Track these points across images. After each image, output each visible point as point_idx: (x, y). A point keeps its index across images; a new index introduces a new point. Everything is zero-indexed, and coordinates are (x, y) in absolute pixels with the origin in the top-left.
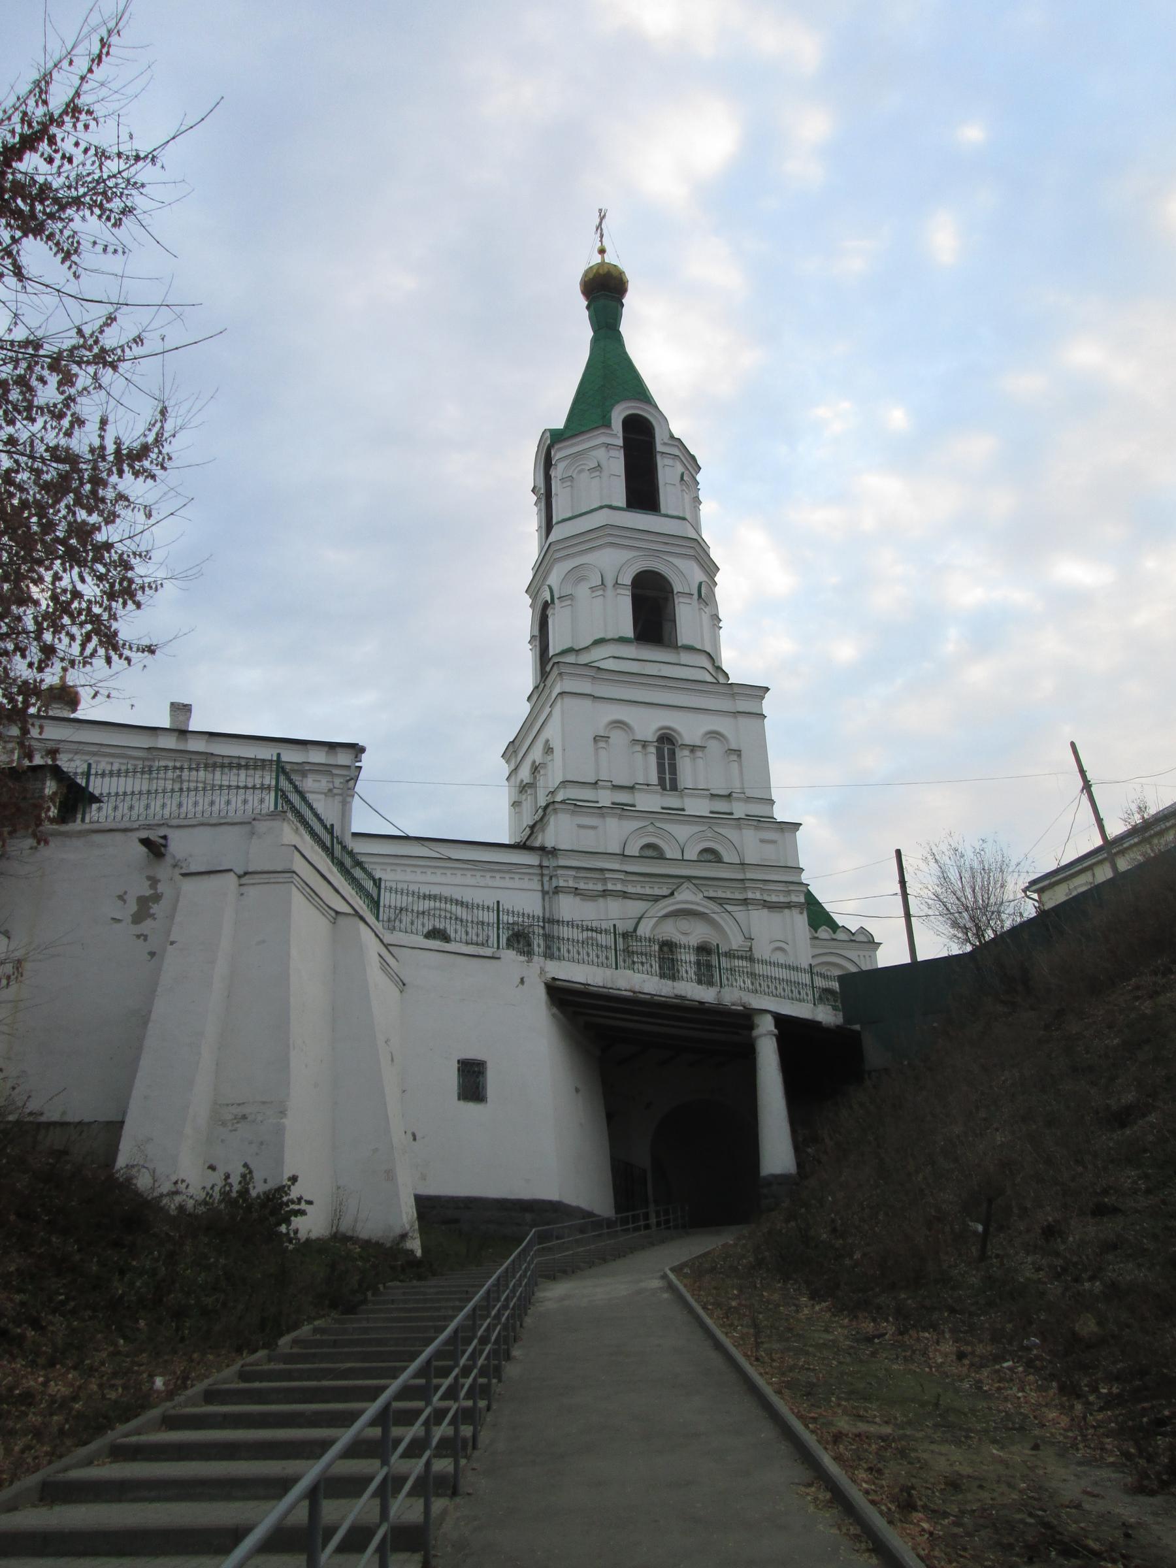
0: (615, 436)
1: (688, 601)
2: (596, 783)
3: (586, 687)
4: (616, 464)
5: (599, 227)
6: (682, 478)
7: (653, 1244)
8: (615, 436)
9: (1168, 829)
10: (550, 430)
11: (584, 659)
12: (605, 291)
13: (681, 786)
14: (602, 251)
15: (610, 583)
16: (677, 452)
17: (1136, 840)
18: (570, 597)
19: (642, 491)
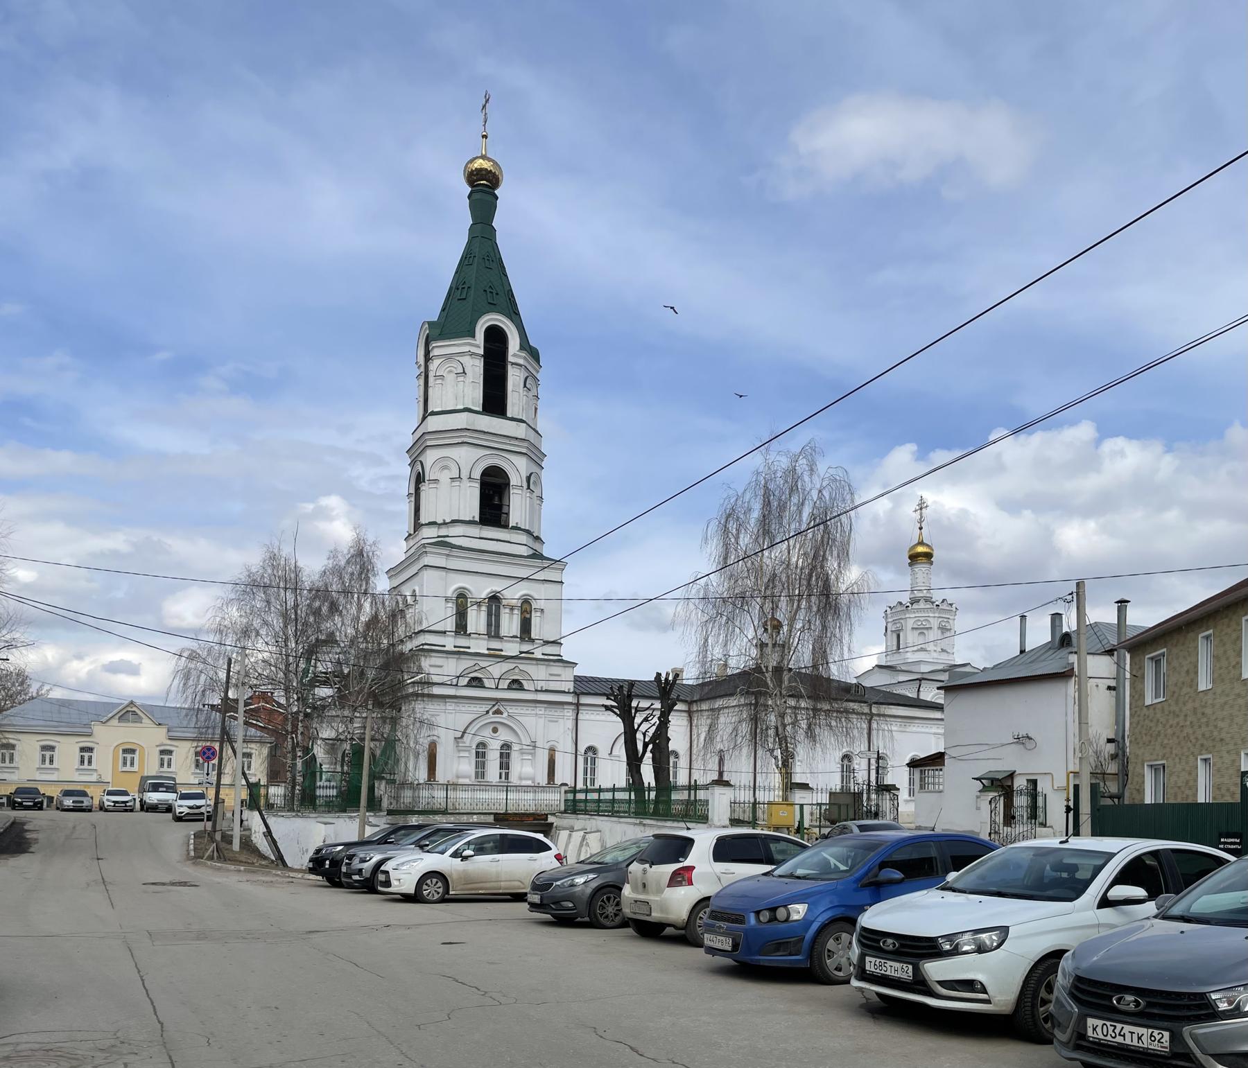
3: (441, 562)
4: (476, 368)
5: (487, 101)
9: (371, 789)
10: (429, 323)
12: (483, 185)
15: (465, 474)
18: (436, 481)
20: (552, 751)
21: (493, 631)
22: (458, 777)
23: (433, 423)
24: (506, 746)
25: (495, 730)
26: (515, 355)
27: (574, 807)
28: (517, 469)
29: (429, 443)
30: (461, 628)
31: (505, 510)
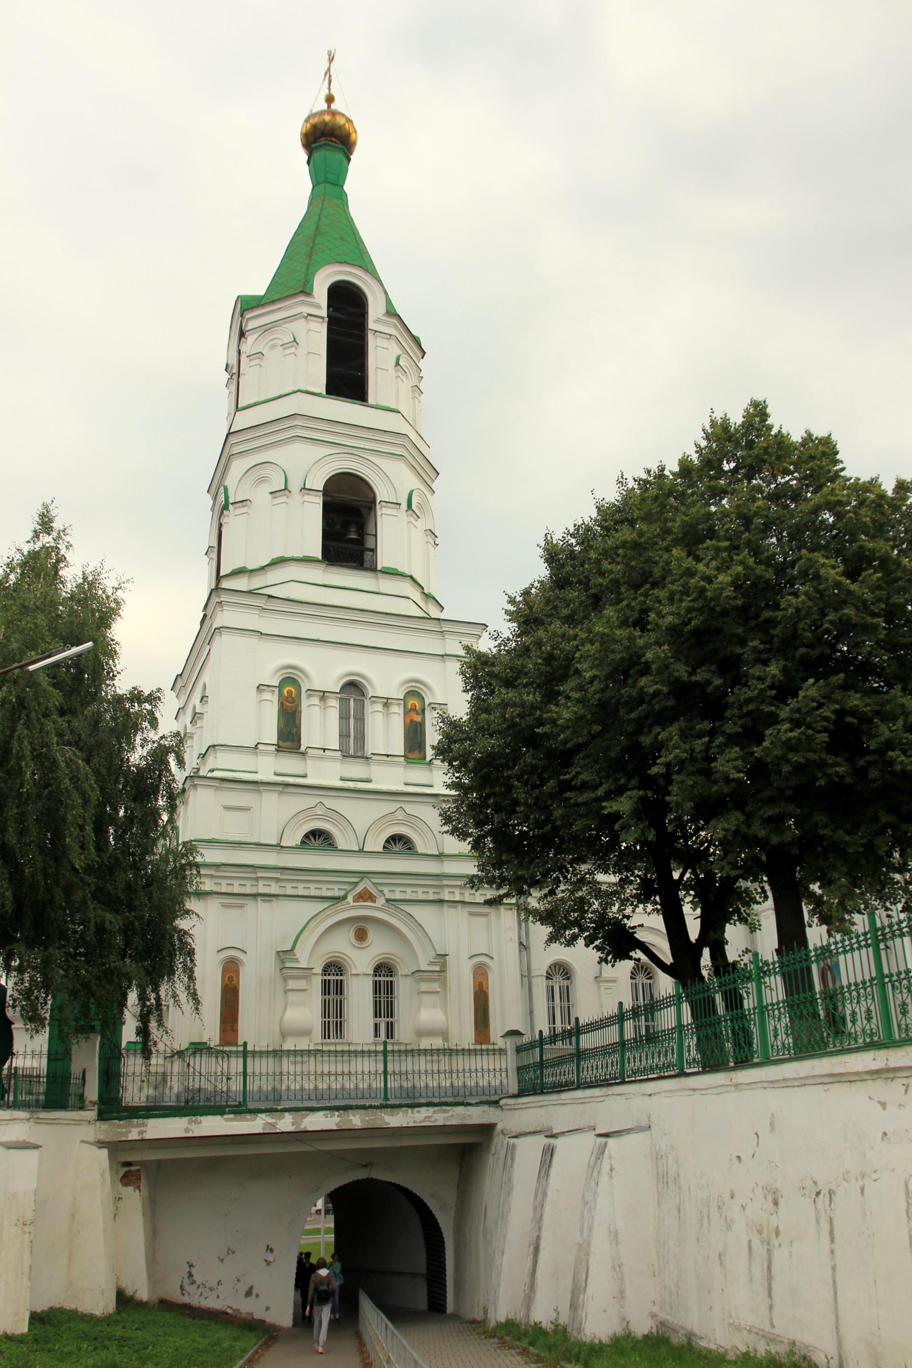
0: (319, 307)
1: (394, 512)
2: (256, 747)
4: (316, 337)
6: (397, 364)
7: (510, 1180)
8: (319, 307)
11: (256, 582)
12: (328, 140)
13: (369, 750)
14: (330, 99)
16: (393, 331)
17: (308, 1308)
19: (347, 375)
20: (481, 973)
21: (353, 744)
22: (284, 1035)
23: (244, 420)
24: (384, 969)
25: (361, 935)
26: (377, 321)
27: (535, 1081)
28: (389, 480)
29: (236, 450)
30: (289, 737)
31: (369, 544)
